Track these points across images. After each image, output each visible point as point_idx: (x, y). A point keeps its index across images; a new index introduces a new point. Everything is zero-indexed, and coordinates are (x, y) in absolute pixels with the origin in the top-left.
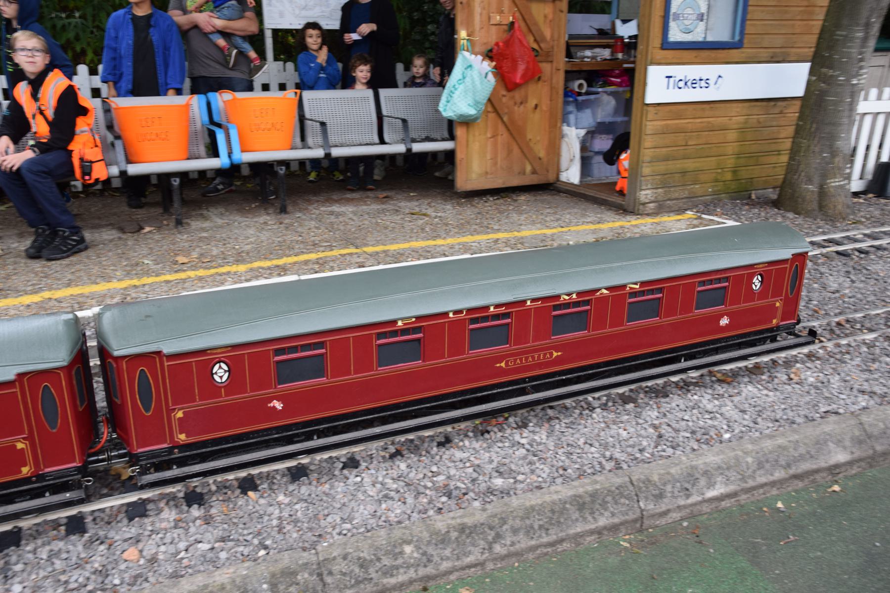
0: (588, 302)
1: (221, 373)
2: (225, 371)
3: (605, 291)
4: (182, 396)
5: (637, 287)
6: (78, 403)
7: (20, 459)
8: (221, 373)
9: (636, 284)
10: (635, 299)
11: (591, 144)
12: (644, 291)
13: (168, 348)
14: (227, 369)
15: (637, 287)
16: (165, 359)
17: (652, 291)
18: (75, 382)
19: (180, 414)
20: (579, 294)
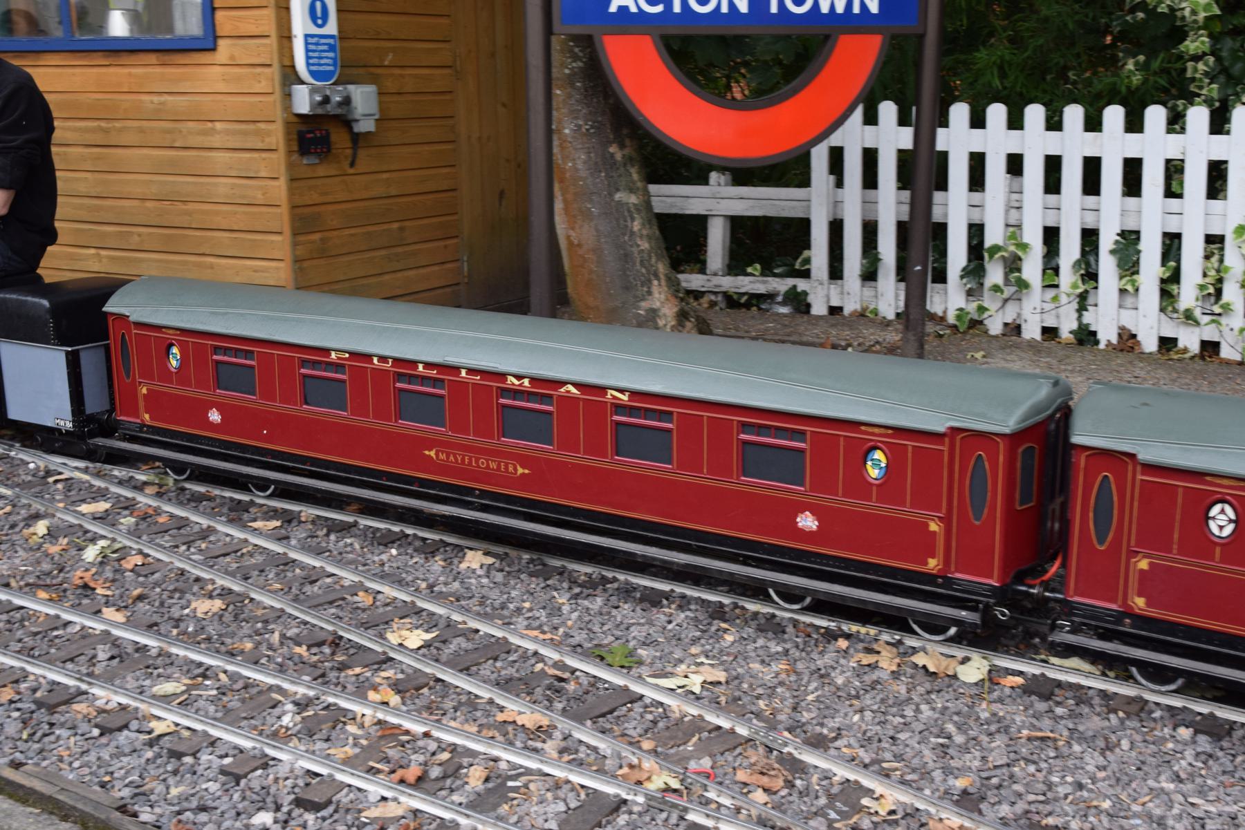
0: (543, 398)
1: (1221, 522)
2: (1230, 521)
3: (573, 390)
4: (1153, 539)
5: (625, 398)
6: (1017, 496)
7: (927, 546)
8: (1221, 522)
9: (621, 391)
10: (234, 360)
11: (1199, 104)
12: (631, 408)
13: (1147, 454)
14: (1233, 517)
15: (625, 398)
16: (1139, 468)
17: (646, 413)
18: (1019, 465)
19: (1144, 564)
20: (534, 380)
